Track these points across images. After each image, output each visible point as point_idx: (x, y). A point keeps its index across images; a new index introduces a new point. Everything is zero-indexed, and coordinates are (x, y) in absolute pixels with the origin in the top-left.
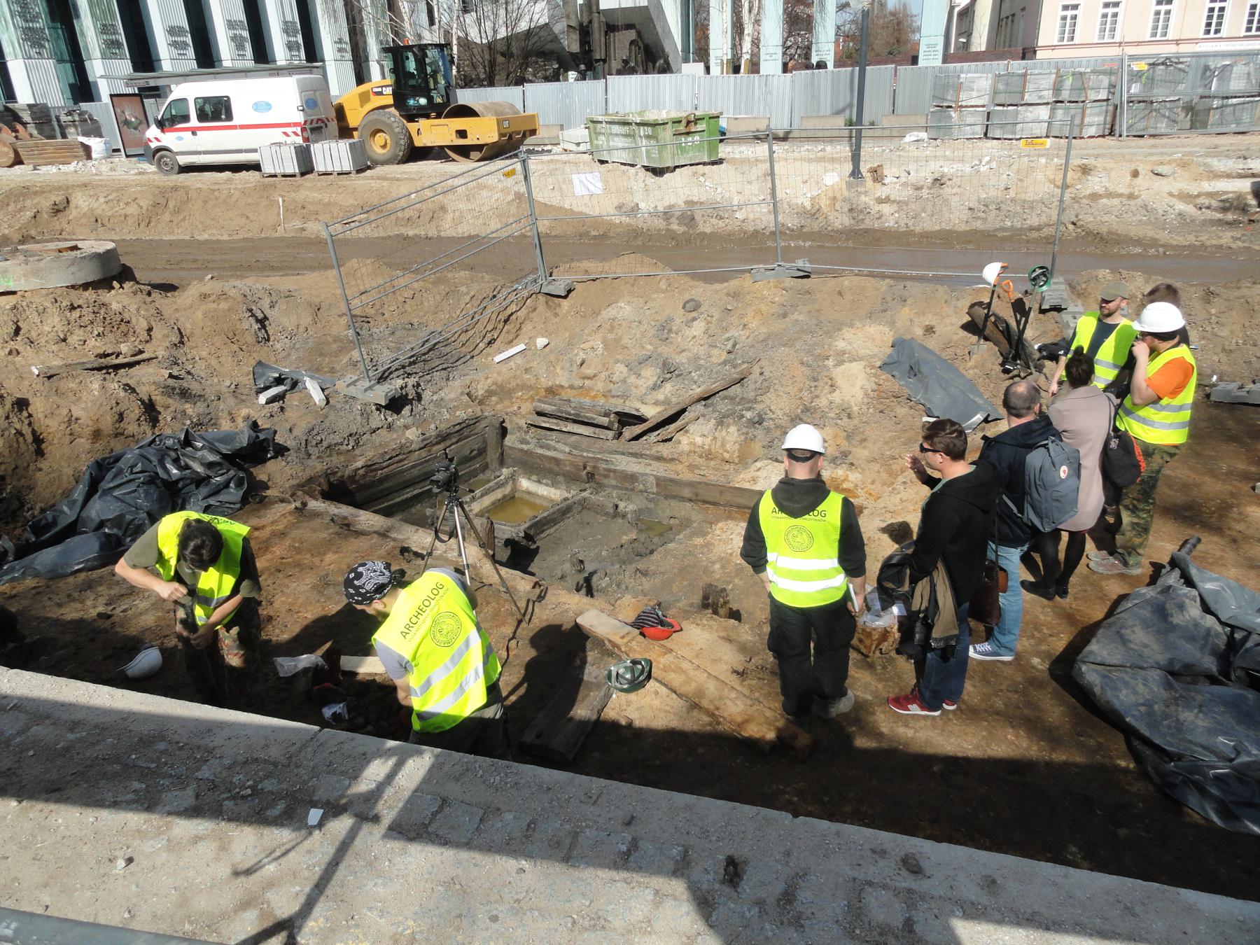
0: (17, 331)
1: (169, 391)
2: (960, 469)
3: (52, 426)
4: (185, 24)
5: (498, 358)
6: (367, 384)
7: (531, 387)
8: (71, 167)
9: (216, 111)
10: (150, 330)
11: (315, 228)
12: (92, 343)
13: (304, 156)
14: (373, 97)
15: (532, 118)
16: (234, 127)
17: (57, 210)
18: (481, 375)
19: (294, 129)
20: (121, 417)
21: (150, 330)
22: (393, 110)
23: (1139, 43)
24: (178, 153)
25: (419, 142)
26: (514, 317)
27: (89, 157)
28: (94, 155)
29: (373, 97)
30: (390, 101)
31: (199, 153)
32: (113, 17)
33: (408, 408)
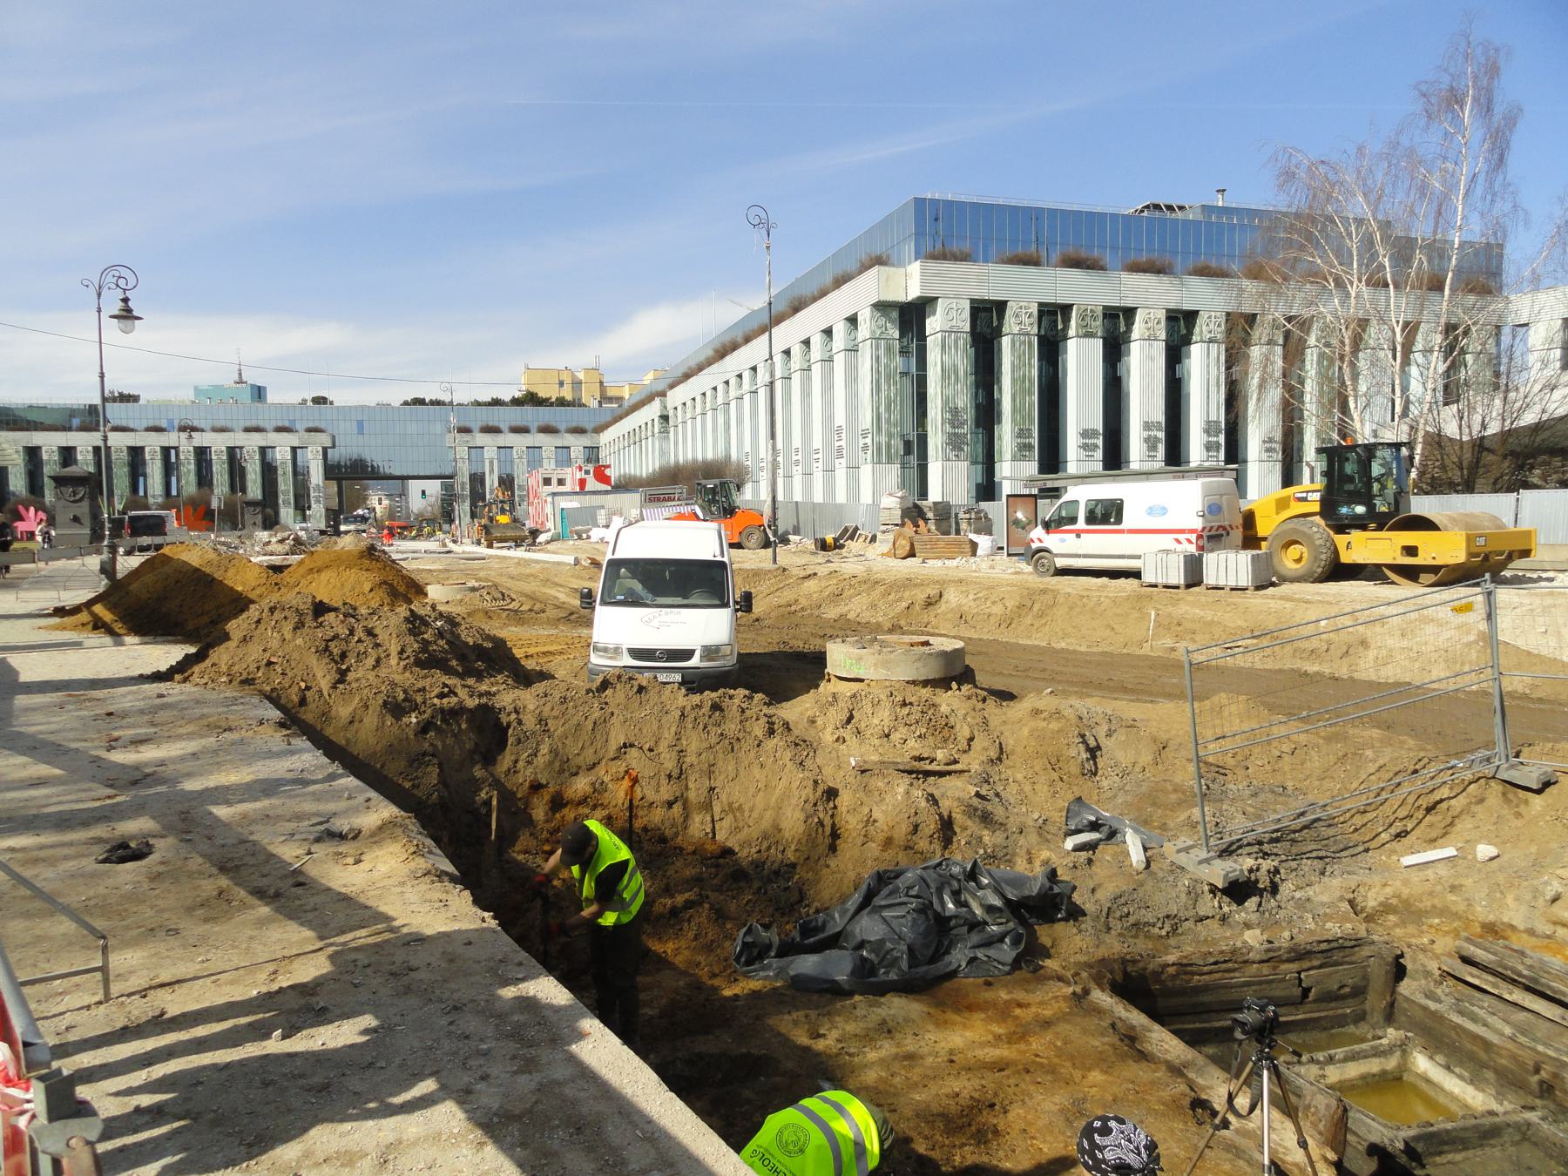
1: (971, 811)
3: (851, 823)
9: (1107, 514)
10: (971, 739)
12: (911, 743)
14: (1293, 503)
17: (930, 603)
18: (1376, 879)
22: (1318, 519)
26: (1444, 805)
27: (974, 554)
29: (1293, 503)
30: (1316, 508)
31: (1085, 556)
32: (1032, 422)
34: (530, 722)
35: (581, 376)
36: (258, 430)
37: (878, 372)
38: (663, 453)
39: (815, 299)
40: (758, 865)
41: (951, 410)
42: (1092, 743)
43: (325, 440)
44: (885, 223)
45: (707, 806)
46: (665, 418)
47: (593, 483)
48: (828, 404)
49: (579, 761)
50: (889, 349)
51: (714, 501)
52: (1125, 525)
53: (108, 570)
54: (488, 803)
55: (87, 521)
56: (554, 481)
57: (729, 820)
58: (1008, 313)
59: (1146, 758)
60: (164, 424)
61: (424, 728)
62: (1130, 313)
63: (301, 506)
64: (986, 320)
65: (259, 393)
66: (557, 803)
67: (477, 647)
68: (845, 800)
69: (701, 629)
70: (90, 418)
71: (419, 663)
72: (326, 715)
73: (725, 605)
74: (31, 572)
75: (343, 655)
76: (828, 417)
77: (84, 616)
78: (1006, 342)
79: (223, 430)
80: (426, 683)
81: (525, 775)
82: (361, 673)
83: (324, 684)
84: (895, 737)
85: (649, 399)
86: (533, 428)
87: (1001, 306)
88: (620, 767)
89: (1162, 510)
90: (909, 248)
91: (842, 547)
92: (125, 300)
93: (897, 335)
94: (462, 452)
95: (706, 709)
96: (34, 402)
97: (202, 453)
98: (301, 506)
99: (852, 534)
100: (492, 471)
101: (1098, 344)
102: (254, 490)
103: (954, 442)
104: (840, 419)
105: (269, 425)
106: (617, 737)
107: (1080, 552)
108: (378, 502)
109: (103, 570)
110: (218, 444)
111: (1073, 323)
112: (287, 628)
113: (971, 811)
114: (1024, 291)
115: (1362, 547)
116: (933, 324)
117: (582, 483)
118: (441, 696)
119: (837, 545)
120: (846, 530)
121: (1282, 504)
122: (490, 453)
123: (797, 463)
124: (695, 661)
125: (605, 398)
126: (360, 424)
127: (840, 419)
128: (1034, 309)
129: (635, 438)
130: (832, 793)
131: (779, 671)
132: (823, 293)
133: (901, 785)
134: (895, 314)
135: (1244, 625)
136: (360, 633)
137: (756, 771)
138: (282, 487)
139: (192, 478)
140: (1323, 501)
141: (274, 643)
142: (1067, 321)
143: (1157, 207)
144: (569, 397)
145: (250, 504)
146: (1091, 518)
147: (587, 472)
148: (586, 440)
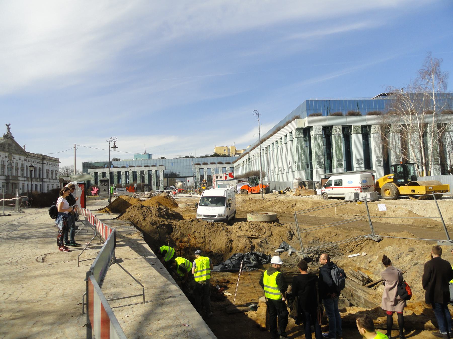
0: (240, 228)
1: (258, 245)
2: (303, 273)
3: (234, 246)
4: (362, 157)
5: (349, 256)
6: (302, 253)
7: (354, 266)
8: (310, 196)
9: (338, 184)
10: (265, 232)
11: (346, 217)
12: (251, 232)
13: (357, 195)
14: (387, 179)
15: (447, 186)
17: (293, 206)
18: (342, 260)
20: (246, 247)
21: (265, 232)
22: (393, 183)
25: (401, 193)
26: (360, 245)
27: (316, 194)
28: (317, 194)
29: (387, 179)
30: (392, 180)
32: (342, 157)
33: (312, 262)
34: (178, 227)
35: (230, 148)
36: (148, 166)
37: (298, 146)
38: (249, 168)
39: (283, 128)
40: (216, 254)
41: (318, 156)
42: (292, 233)
43: (164, 168)
44: (299, 108)
45: (209, 244)
46: (249, 159)
47: (228, 178)
48: (287, 155)
49: (186, 234)
50: (301, 140)
51: (253, 182)
53: (109, 201)
54: (168, 241)
55: (107, 190)
56: (219, 177)
57: (212, 247)
58: (333, 129)
59: (303, 236)
60: (126, 166)
61: (157, 227)
62: (370, 126)
63: (158, 185)
64: (327, 131)
65: (150, 156)
66: (181, 242)
67: (171, 214)
68: (234, 242)
69: (219, 211)
70: (109, 165)
71: (159, 216)
72: (141, 225)
73: (224, 206)
74: (94, 202)
75: (145, 215)
76: (287, 158)
77: (104, 210)
78: (333, 136)
79: (139, 167)
80: (159, 220)
81: (176, 236)
82: (148, 218)
83: (141, 220)
84: (249, 231)
85: (245, 154)
86: (216, 163)
87: (331, 127)
88: (193, 236)
89: (352, 182)
90: (305, 113)
91: (285, 193)
92: (114, 144)
93: (303, 136)
94: (198, 170)
95: (210, 225)
96: (97, 161)
97: (134, 172)
98: (158, 185)
99: (288, 190)
100: (206, 175)
101: (360, 135)
102: (146, 182)
103: (319, 164)
104: (290, 159)
105: (150, 165)
106: (193, 230)
108: (179, 184)
109: (109, 201)
110: (138, 170)
111: (353, 130)
112: (136, 210)
113: (258, 245)
114: (337, 123)
115: (404, 190)
116: (312, 133)
117: (226, 177)
118: (161, 222)
119: (284, 193)
120: (287, 188)
121: (385, 180)
122: (205, 170)
123: (280, 171)
124: (216, 217)
125: (237, 154)
126: (172, 163)
127: (290, 159)
128: (341, 127)
129: (242, 165)
130: (231, 241)
131: (231, 220)
132: (285, 126)
133: (245, 239)
134: (302, 131)
135: (359, 210)
136: (149, 211)
137: (219, 237)
138: (153, 180)
139: (132, 179)
140: (394, 178)
141: (133, 213)
142: (351, 130)
143: (384, 95)
144: (227, 154)
145: (145, 185)
146: (335, 185)
147: (227, 175)
148: (230, 166)
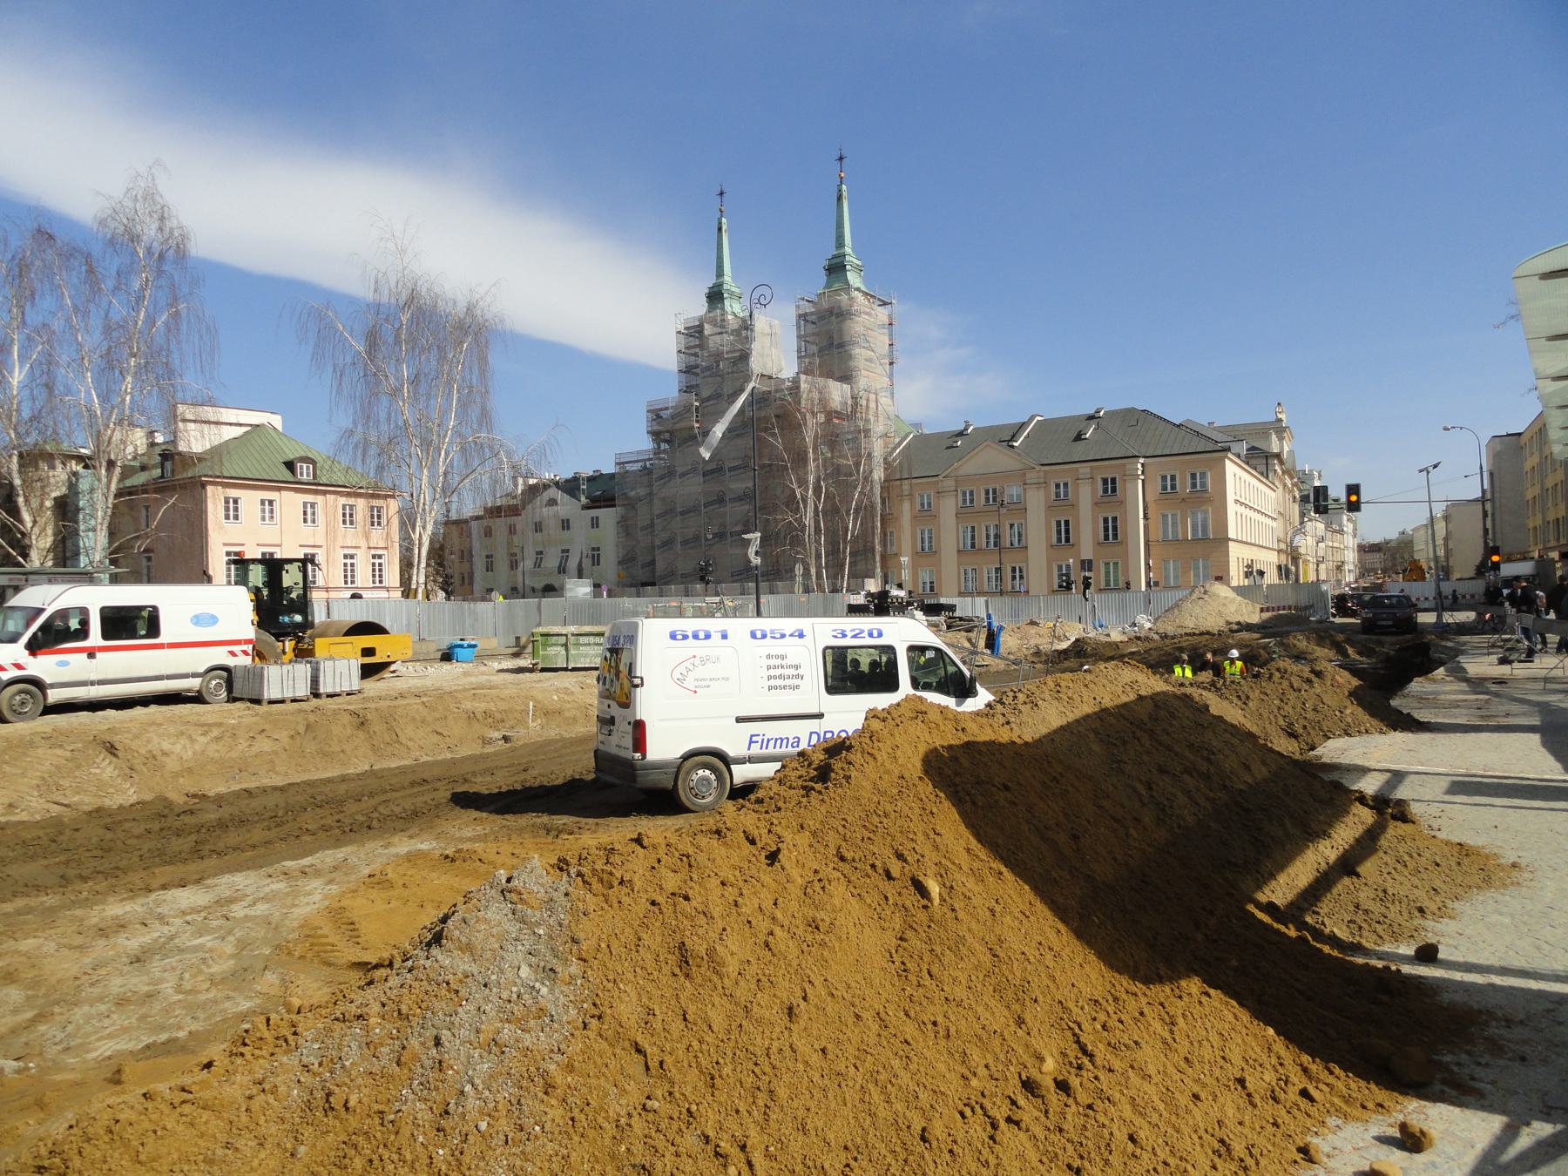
16: (161, 646)
19: (244, 647)
23: (1347, 865)
24: (53, 686)
31: (169, 677)
52: (164, 638)
107: (94, 677)
